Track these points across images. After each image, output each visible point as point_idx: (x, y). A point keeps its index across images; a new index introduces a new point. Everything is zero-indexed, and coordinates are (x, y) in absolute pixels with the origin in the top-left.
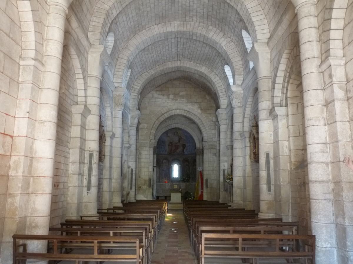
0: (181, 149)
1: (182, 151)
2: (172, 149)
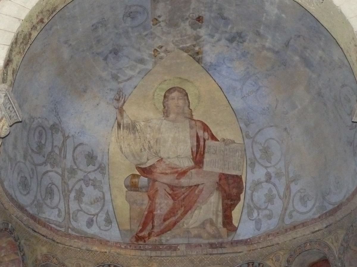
0: (210, 207)
1: (220, 220)
2: (151, 212)
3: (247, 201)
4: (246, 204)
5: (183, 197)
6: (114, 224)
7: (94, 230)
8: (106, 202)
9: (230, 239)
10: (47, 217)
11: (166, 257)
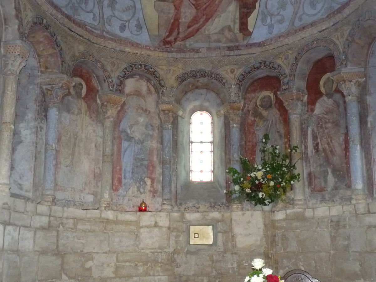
1: (237, 26)
2: (177, 20)
3: (261, 9)
4: (260, 11)
5: (205, 6)
6: (144, 30)
7: (126, 34)
8: (136, 10)
9: (245, 42)
10: (83, 20)
11: (189, 58)
